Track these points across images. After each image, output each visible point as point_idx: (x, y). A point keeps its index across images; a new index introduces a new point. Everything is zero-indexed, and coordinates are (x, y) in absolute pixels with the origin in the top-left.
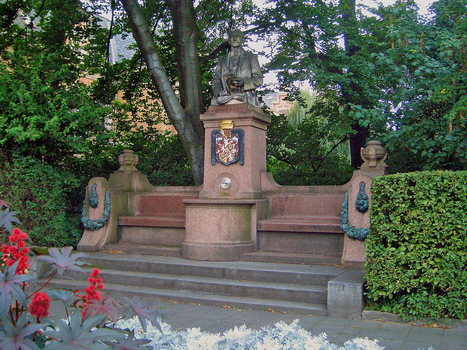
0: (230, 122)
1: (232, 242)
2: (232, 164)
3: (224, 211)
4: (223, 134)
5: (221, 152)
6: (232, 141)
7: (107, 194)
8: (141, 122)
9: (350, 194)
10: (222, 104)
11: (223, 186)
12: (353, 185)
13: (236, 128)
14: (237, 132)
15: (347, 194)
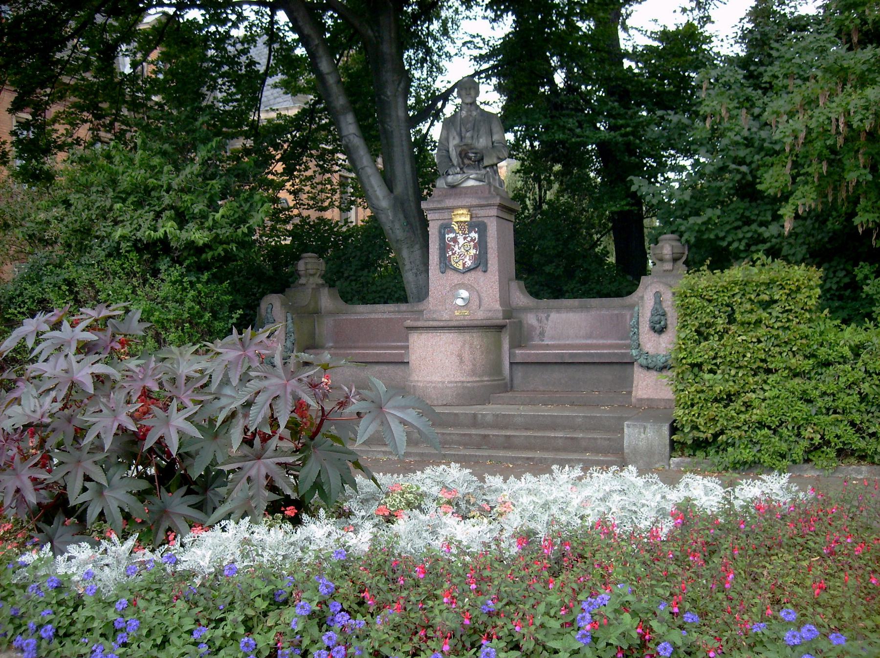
0: (465, 211)
1: (478, 379)
2: (470, 270)
3: (467, 336)
4: (456, 228)
5: (453, 254)
6: (469, 239)
7: (289, 318)
8: (307, 209)
9: (641, 308)
10: (453, 187)
11: (460, 302)
12: (646, 297)
13: (474, 220)
14: (476, 226)
15: (636, 308)
